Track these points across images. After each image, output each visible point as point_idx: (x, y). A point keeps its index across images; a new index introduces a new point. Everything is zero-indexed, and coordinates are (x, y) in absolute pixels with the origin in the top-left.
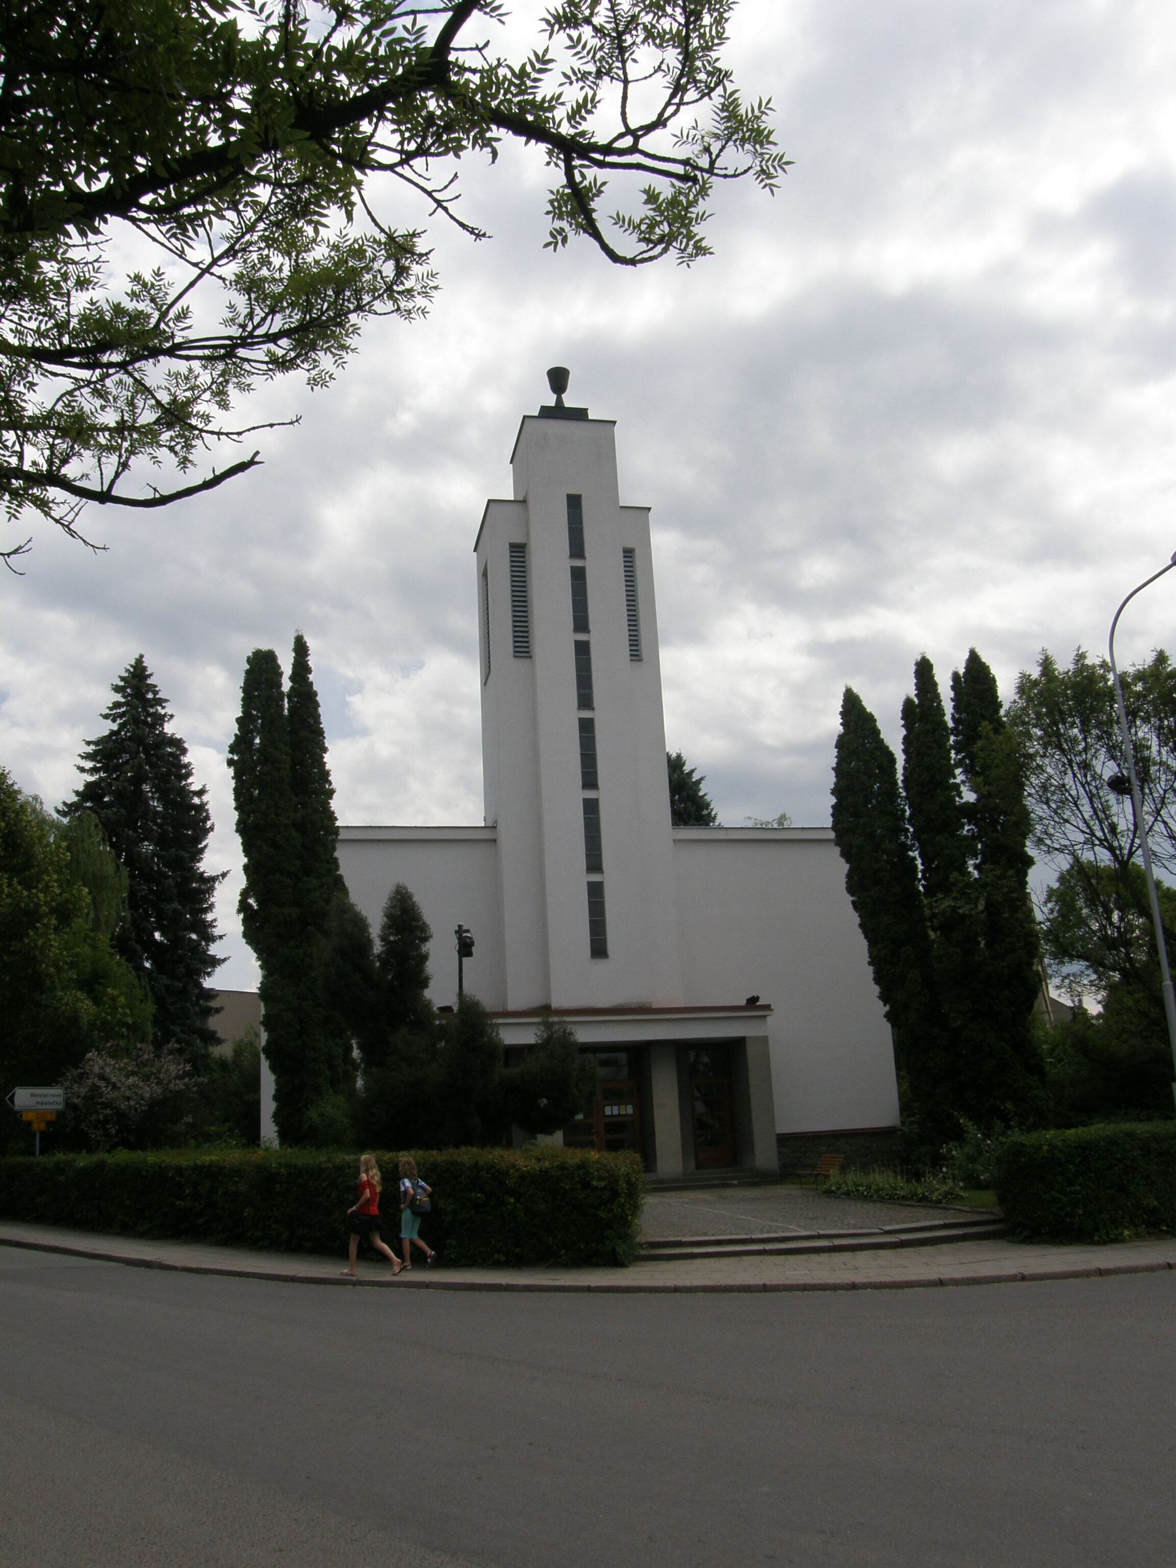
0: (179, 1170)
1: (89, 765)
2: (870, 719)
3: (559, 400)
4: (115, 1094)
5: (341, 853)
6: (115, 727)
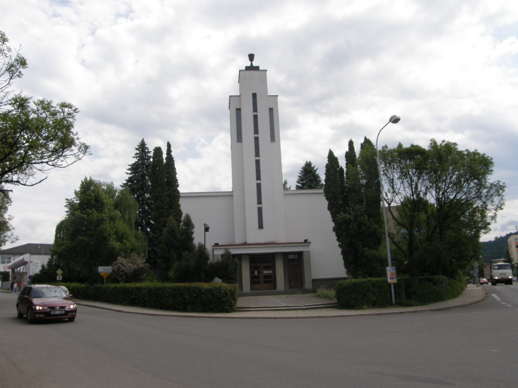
0: (132, 288)
1: (130, 172)
2: (336, 159)
3: (252, 64)
4: (125, 268)
5: (181, 202)
6: (137, 161)
